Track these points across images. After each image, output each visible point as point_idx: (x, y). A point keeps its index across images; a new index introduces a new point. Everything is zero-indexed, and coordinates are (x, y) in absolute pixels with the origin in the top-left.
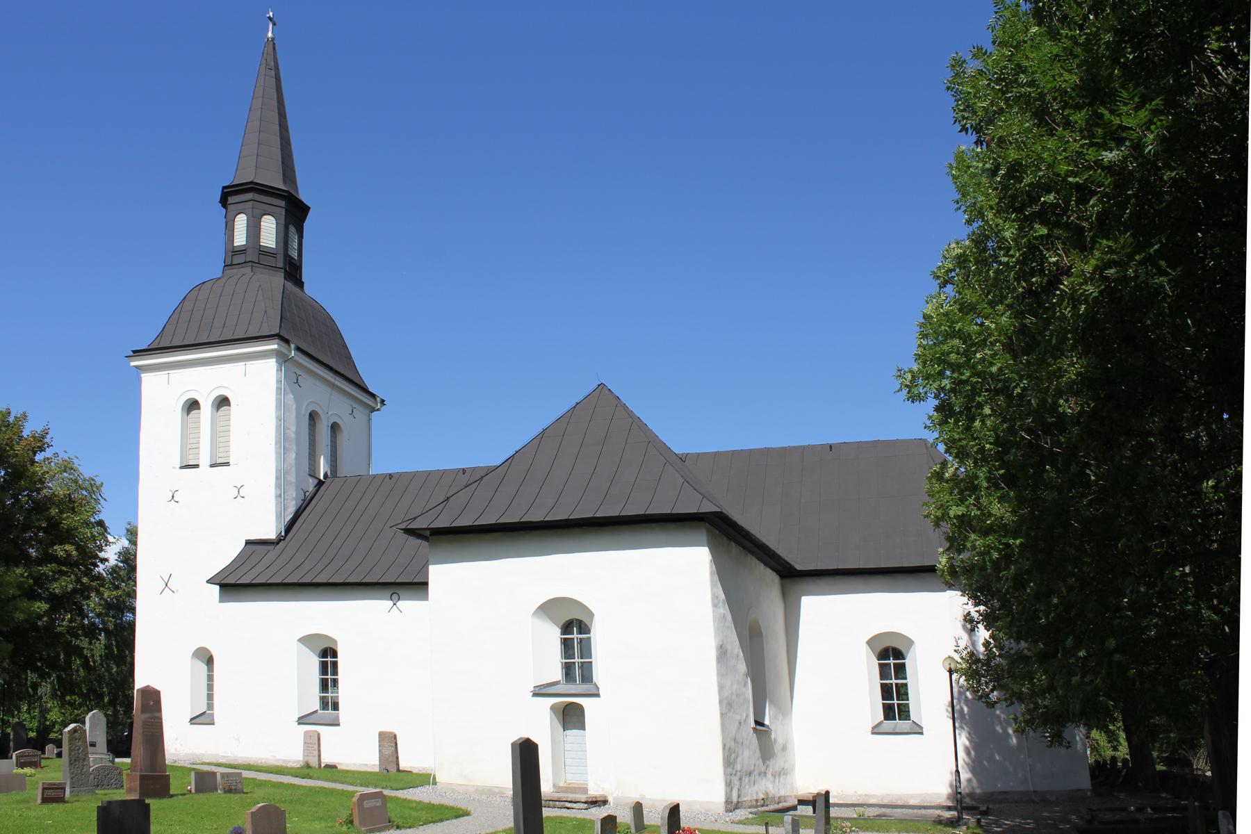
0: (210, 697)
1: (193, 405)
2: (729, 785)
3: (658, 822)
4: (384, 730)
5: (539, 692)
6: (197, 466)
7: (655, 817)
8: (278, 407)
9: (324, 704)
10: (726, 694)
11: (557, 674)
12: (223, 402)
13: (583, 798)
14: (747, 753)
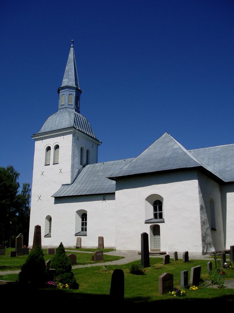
0: (50, 229)
1: (49, 149)
2: (203, 247)
3: (182, 258)
4: (99, 236)
5: (146, 222)
6: (49, 165)
7: (181, 257)
8: (72, 147)
9: (82, 229)
10: (203, 220)
11: (152, 216)
12: (57, 147)
13: (158, 252)
14: (209, 238)
